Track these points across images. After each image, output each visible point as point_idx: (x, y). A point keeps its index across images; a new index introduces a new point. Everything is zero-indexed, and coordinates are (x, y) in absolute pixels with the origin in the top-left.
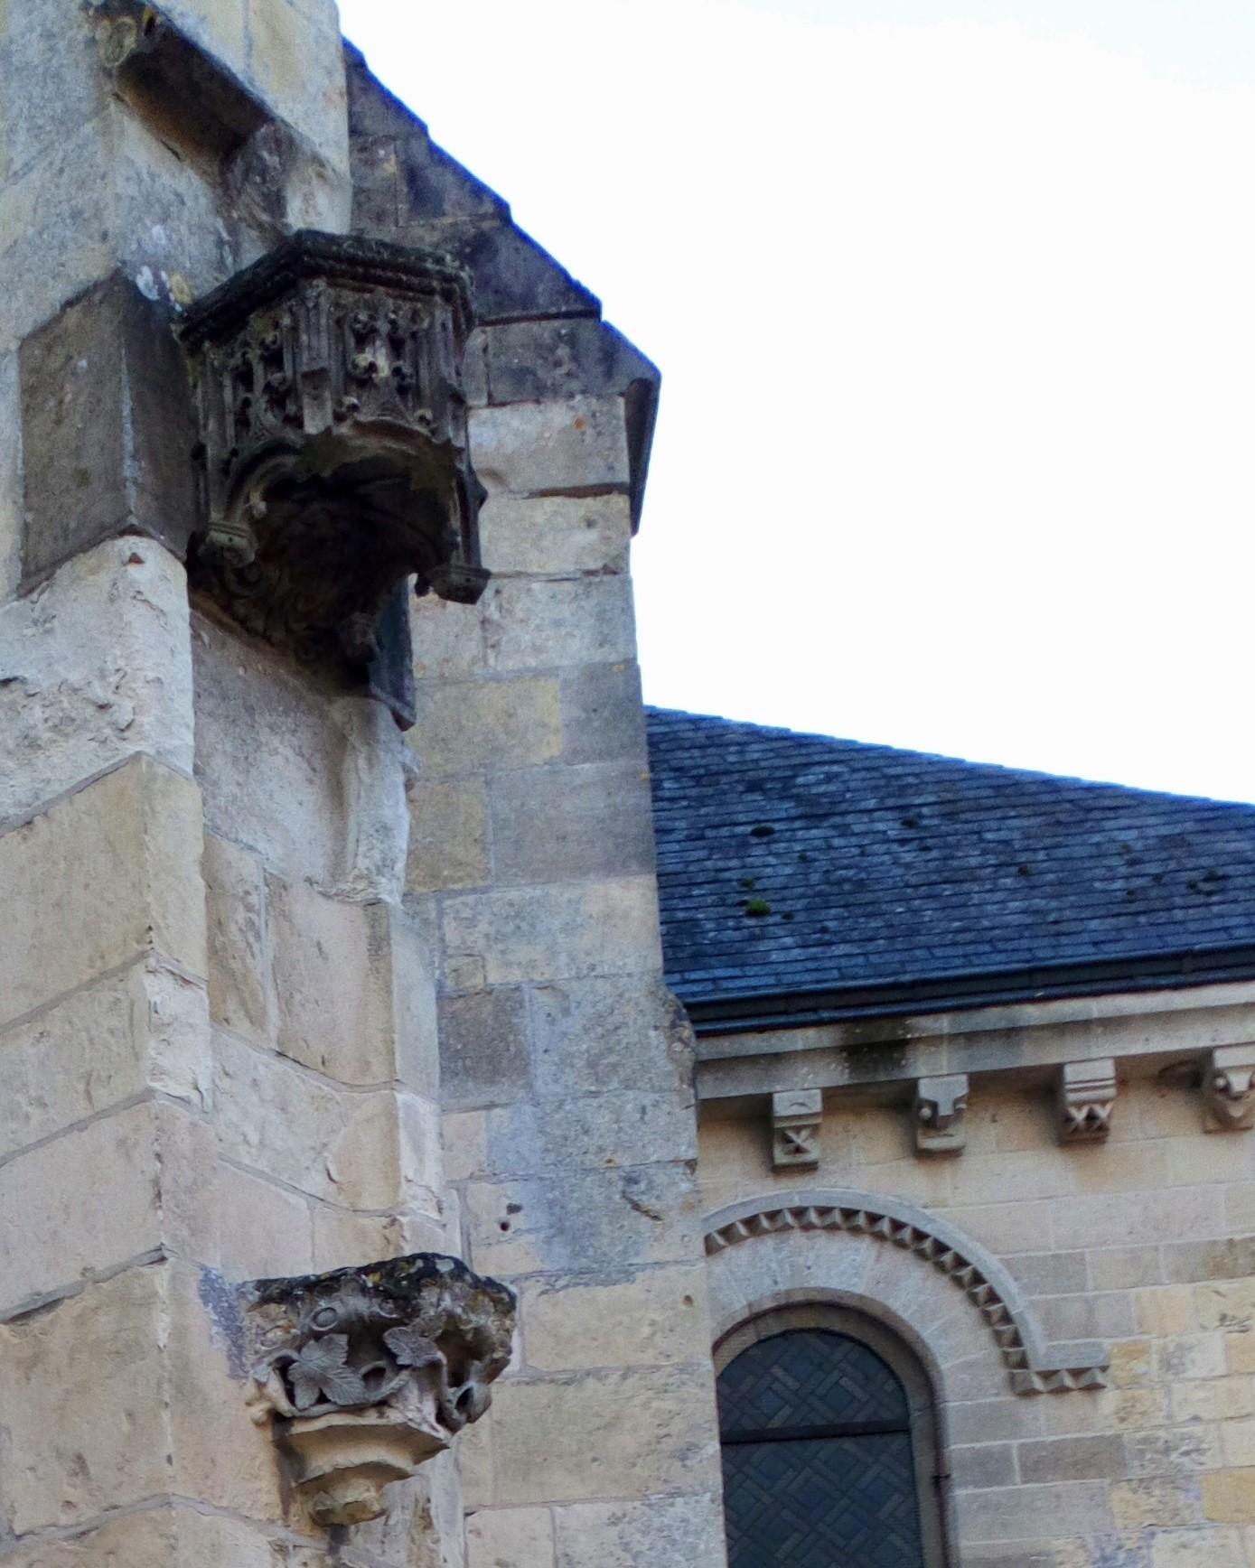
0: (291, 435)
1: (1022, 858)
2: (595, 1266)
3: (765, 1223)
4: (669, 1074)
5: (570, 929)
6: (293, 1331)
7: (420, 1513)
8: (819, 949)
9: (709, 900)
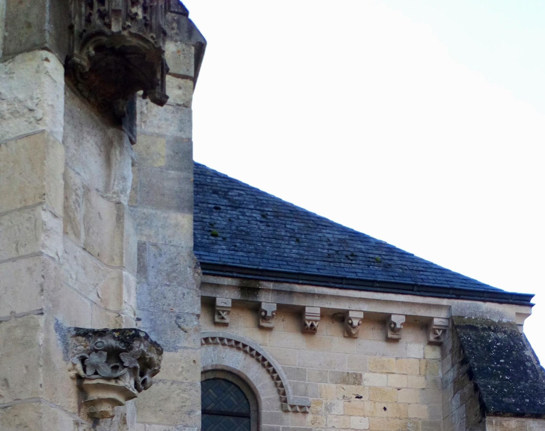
0: (106, 30)
1: (298, 236)
2: (165, 344)
3: (210, 341)
4: (193, 284)
5: (163, 227)
6: (87, 347)
7: (122, 418)
8: (233, 252)
9: (199, 227)
